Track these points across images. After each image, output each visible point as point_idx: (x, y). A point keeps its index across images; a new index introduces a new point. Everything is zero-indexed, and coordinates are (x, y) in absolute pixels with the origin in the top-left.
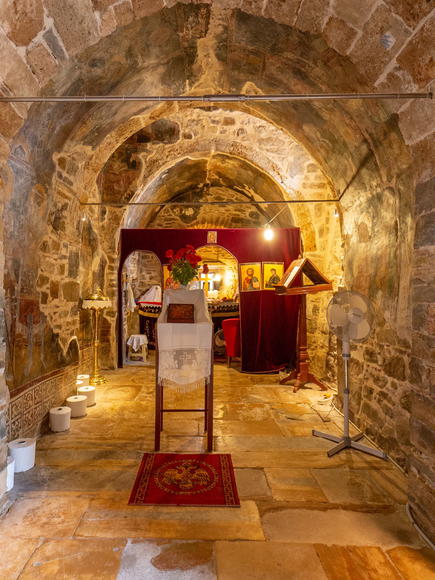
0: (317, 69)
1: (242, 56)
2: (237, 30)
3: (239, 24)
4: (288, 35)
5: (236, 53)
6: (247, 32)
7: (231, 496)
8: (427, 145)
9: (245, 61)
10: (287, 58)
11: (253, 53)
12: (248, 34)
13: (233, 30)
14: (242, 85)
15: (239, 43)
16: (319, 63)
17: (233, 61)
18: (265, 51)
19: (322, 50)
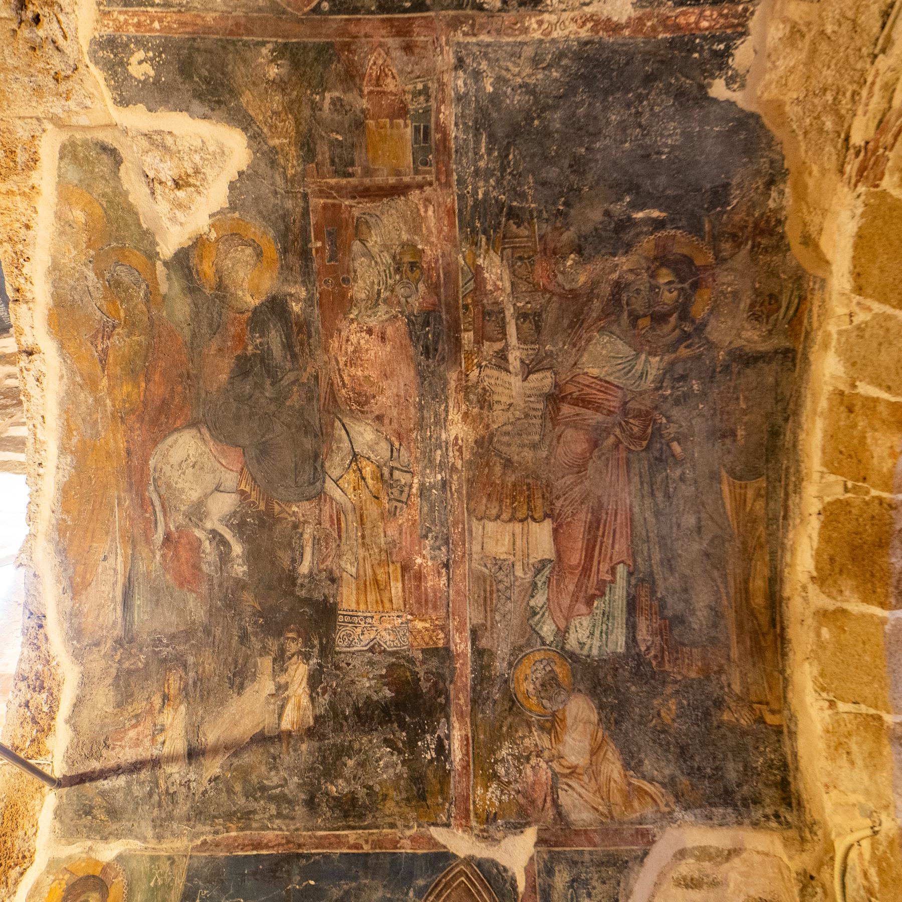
0: (516, 382)
1: (390, 85)
2: (528, 52)
3: (562, 55)
4: (579, 250)
5: (397, 54)
6: (533, 92)
7: (466, 307)
8: (640, 803)
9: (364, 103)
10: (477, 271)
11: (423, 134)
12: (516, 100)
13: (525, 30)
14: (196, 105)
15: (460, 64)
16: (543, 381)
17: (347, 46)
18: (461, 182)
19: (595, 372)
